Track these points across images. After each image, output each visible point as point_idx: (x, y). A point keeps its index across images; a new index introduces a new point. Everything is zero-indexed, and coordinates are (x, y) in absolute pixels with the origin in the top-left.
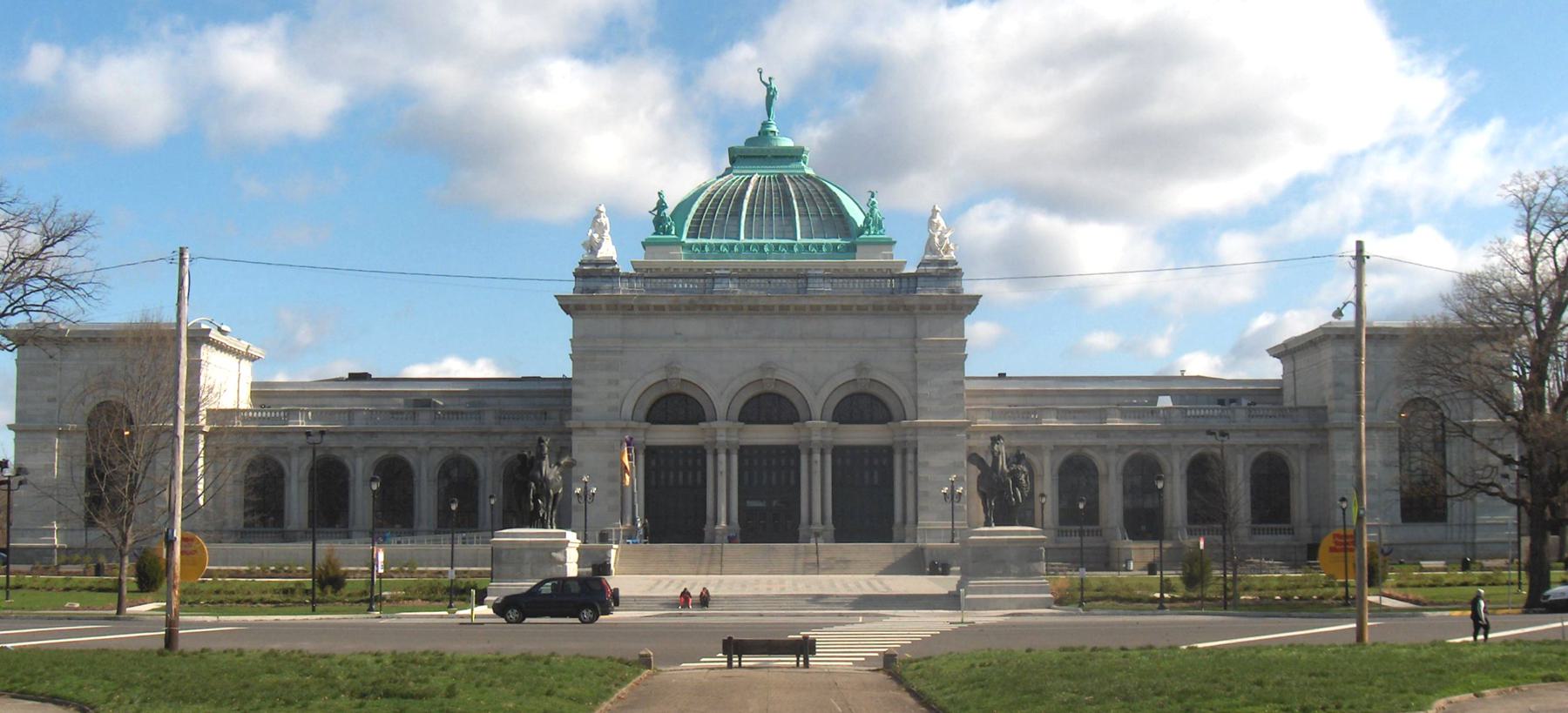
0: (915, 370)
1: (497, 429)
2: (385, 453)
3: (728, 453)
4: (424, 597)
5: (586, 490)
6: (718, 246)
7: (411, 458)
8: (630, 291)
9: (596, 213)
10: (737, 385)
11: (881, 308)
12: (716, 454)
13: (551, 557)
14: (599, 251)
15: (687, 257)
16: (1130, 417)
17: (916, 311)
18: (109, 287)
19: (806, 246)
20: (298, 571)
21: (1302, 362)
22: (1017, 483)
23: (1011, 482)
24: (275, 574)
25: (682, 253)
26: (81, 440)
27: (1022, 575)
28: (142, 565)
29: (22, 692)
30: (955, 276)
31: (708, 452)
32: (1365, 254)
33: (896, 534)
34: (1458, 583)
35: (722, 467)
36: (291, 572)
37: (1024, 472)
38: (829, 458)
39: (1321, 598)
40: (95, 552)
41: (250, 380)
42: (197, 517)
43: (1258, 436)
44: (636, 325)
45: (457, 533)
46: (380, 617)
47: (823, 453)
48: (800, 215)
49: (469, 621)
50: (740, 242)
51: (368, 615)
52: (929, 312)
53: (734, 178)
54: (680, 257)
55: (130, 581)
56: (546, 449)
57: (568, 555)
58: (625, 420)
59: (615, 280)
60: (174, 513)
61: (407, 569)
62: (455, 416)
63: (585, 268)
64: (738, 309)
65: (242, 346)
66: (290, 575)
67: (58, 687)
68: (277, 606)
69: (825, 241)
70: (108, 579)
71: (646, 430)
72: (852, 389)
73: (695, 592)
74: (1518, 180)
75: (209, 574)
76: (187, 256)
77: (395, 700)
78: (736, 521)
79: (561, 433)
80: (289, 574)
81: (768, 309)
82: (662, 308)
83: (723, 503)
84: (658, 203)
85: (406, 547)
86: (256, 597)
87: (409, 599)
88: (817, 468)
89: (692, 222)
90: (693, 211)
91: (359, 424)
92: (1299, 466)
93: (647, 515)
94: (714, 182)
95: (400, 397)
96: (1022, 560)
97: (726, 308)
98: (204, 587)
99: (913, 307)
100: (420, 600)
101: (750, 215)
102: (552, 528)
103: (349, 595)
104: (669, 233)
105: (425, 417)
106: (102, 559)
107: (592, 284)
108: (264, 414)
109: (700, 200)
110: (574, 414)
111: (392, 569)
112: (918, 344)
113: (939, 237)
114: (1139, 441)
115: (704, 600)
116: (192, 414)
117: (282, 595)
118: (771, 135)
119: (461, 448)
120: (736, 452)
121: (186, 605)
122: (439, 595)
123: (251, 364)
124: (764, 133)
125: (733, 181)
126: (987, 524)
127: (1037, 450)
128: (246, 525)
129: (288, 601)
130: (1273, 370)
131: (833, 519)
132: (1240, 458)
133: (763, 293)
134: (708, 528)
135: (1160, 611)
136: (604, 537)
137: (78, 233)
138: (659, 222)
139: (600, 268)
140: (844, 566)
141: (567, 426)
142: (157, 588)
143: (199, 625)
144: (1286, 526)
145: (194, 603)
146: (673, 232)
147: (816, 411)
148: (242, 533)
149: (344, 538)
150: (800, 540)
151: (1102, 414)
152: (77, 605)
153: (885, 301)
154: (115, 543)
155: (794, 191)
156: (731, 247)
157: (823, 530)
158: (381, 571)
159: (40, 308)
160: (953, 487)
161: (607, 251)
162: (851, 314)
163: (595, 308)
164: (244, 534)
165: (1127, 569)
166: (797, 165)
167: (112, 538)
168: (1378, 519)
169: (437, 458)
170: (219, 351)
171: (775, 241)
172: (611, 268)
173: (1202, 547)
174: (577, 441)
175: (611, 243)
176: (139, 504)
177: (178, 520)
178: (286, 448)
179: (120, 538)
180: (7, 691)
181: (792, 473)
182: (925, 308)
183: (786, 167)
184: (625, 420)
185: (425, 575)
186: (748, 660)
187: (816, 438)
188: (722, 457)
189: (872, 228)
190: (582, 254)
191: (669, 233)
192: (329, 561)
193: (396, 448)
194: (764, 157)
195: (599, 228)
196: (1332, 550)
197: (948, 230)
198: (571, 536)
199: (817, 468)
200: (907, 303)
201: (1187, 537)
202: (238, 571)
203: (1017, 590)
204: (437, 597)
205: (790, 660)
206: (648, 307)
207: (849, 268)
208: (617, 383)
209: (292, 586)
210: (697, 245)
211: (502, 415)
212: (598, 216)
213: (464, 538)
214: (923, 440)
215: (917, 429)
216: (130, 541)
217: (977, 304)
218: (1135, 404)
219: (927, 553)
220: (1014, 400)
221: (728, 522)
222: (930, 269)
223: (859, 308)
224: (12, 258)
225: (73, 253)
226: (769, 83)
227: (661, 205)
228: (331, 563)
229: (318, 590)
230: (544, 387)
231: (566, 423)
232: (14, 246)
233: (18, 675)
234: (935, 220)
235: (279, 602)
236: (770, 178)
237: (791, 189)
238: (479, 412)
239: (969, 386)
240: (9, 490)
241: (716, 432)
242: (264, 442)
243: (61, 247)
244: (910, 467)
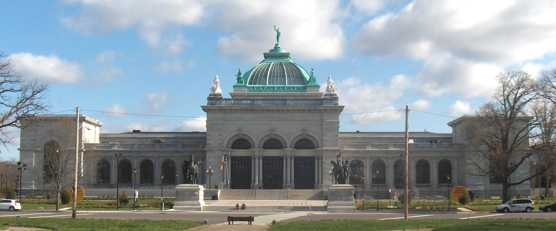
1: (182, 150)
2: (143, 158)
3: (259, 159)
4: (153, 206)
5: (210, 172)
6: (259, 87)
7: (153, 160)
8: (226, 104)
9: (215, 78)
10: (262, 136)
11: (311, 110)
12: (255, 159)
13: (194, 193)
14: (216, 91)
15: (248, 91)
16: (396, 147)
17: (323, 111)
18: (53, 107)
19: (289, 87)
20: (115, 198)
21: (458, 128)
22: (345, 170)
23: (343, 170)
24: (107, 199)
25: (246, 89)
26: (42, 154)
27: (346, 200)
28: (63, 196)
29: (38, 226)
30: (336, 100)
32: (408, 109)
34: (493, 204)
35: (257, 164)
36: (112, 198)
37: (348, 167)
38: (293, 161)
39: (442, 208)
40: (47, 191)
41: (99, 133)
42: (81, 180)
43: (440, 154)
44: (228, 116)
45: (164, 185)
46: (136, 212)
47: (291, 159)
49: (162, 212)
51: (133, 211)
52: (327, 111)
53: (266, 63)
54: (246, 91)
55: (60, 201)
56: (193, 159)
57: (200, 193)
58: (224, 148)
59: (221, 101)
60: (75, 181)
61: (150, 197)
62: (168, 146)
63: (211, 97)
64: (262, 111)
65: (96, 122)
66: (111, 199)
67: (47, 225)
68: (106, 208)
69: (295, 86)
70: (52, 200)
71: (231, 151)
72: (301, 138)
73: (240, 205)
74: (501, 74)
75: (85, 199)
76: (79, 109)
77: (129, 227)
78: (262, 182)
79: (203, 152)
80: (111, 199)
81: (273, 111)
82: (237, 110)
83: (257, 176)
85: (148, 190)
86: (100, 206)
87: (149, 207)
88: (289, 164)
90: (251, 75)
91: (135, 148)
92: (455, 164)
93: (232, 180)
94: (258, 65)
95: (150, 139)
96: (346, 195)
97: (258, 110)
98: (83, 203)
99: (321, 110)
100: (152, 207)
101: (270, 77)
102: (195, 184)
103: (129, 205)
104: (242, 83)
105: (157, 146)
106: (49, 194)
107: (213, 102)
108: (105, 145)
109: (253, 71)
110: (207, 146)
111: (146, 197)
112: (323, 122)
113: (331, 86)
115: (244, 207)
116: (80, 145)
117: (108, 206)
118: (278, 48)
119: (169, 157)
121: (77, 208)
122: (158, 206)
123: (99, 127)
124: (276, 48)
125: (265, 65)
126: (336, 184)
127: (364, 158)
128: (97, 183)
129: (110, 207)
130: (449, 130)
131: (294, 181)
132: (434, 161)
133: (271, 105)
135: (378, 211)
136: (216, 187)
137: (44, 90)
138: (239, 79)
139: (216, 96)
140: (296, 197)
141: (205, 150)
142: (68, 203)
143: (81, 213)
144: (428, 184)
145: (80, 208)
146: (244, 83)
147: (289, 145)
148: (96, 185)
149: (130, 187)
150: (315, 188)
151: (387, 146)
152: (43, 208)
153: (312, 108)
154: (56, 189)
155: (286, 68)
156: (263, 88)
157: (291, 185)
158: (137, 197)
159: (32, 116)
161: (219, 91)
162: (301, 112)
163: (214, 110)
164: (96, 186)
165: (393, 199)
167: (55, 187)
168: (481, 182)
169: (161, 160)
170: (88, 124)
171: (279, 86)
172: (220, 96)
173: (390, 192)
174: (208, 155)
175: (220, 88)
176: (63, 176)
177: (76, 183)
178: (111, 157)
179: (57, 187)
180: (33, 226)
182: (325, 110)
183: (283, 60)
184: (224, 148)
185: (157, 199)
186: (235, 223)
187: (289, 154)
188: (257, 160)
189: (312, 81)
190: (210, 92)
191: (242, 83)
192: (123, 195)
193: (148, 157)
195: (216, 83)
196: (455, 193)
197: (334, 84)
198: (201, 187)
199: (289, 164)
200: (319, 109)
201: (415, 188)
202: (94, 198)
203: (344, 205)
204: (158, 206)
205: (247, 223)
206: (232, 110)
207: (304, 95)
208: (221, 135)
209: (112, 203)
210: (252, 87)
211: (183, 146)
212: (216, 79)
213: (170, 187)
214: (324, 155)
215: (322, 151)
216: (60, 188)
217: (343, 109)
218: (401, 142)
220: (360, 141)
221: (259, 182)
222: (328, 97)
223: (303, 110)
224: (23, 99)
225: (42, 97)
227: (239, 74)
228: (124, 195)
229: (119, 204)
230: (199, 136)
231: (204, 148)
232: (23, 95)
233: (36, 223)
234: (329, 80)
235: (107, 208)
236: (277, 64)
237: (284, 67)
238: (176, 145)
239: (340, 135)
240: (21, 171)
241: (255, 152)
242: (104, 155)
243: (38, 95)
244: (320, 164)
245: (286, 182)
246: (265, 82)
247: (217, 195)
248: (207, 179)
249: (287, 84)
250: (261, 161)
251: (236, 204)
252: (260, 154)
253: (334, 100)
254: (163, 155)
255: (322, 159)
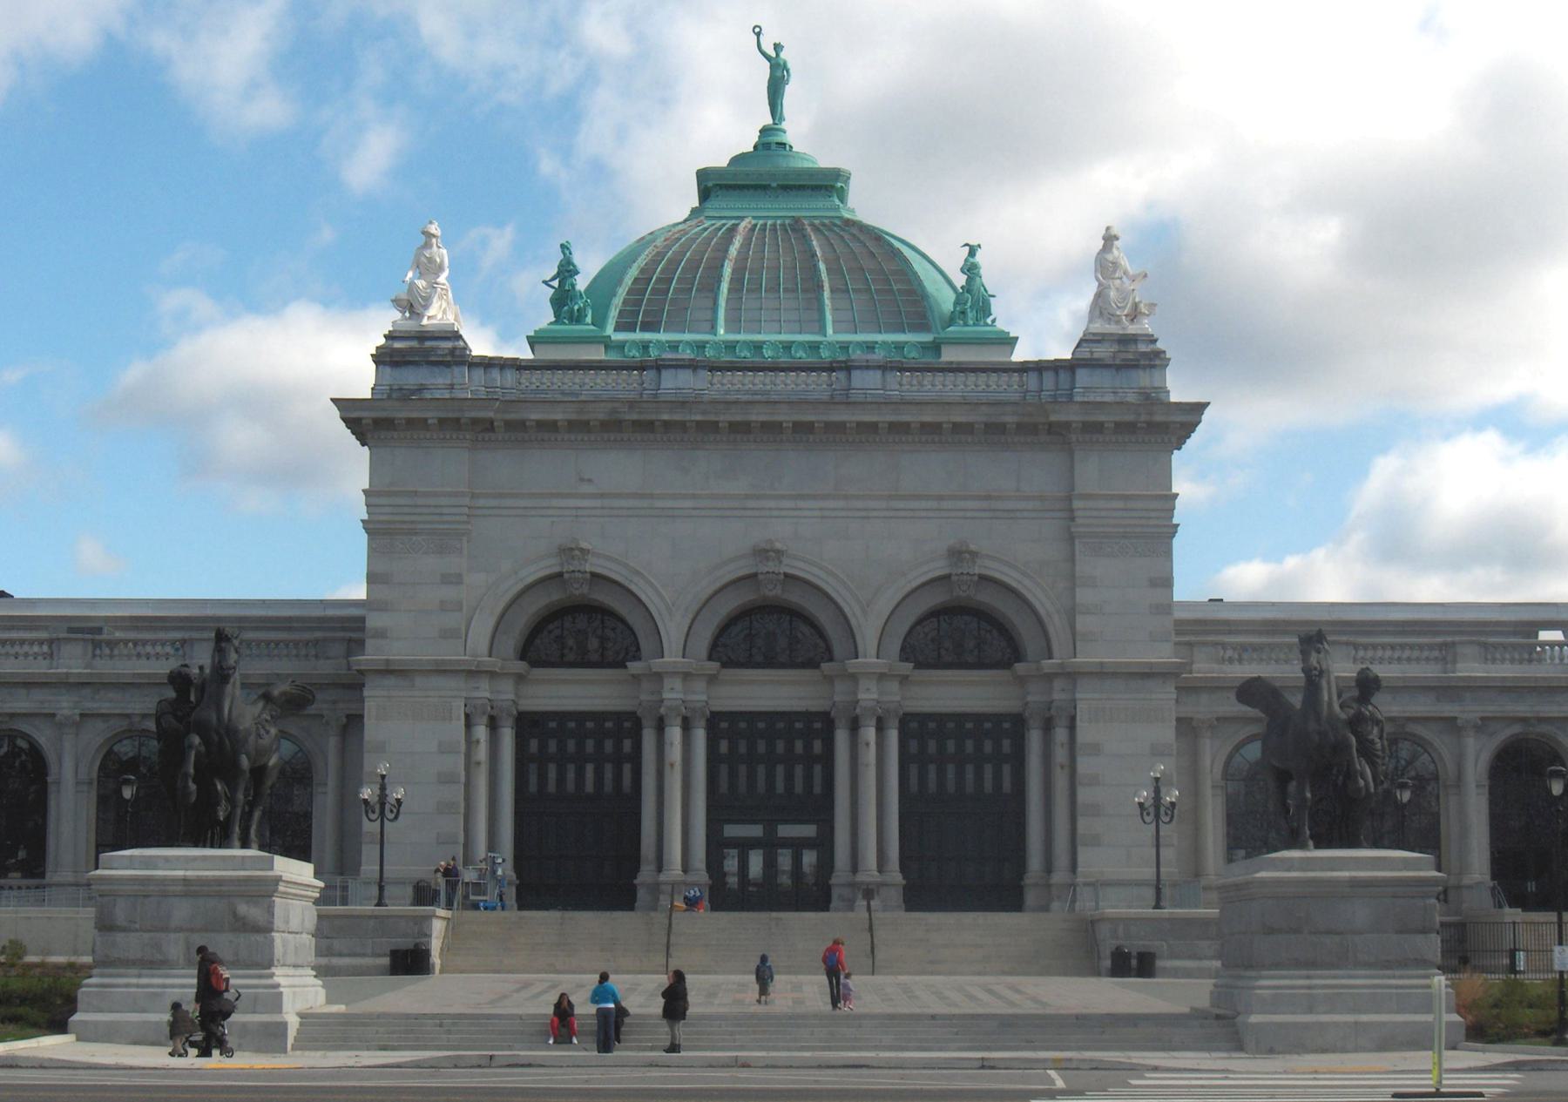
0: (1072, 559)
3: (687, 726)
10: (707, 587)
30: (1153, 366)
31: (644, 722)
33: (1030, 897)
35: (675, 753)
38: (893, 736)
48: (832, 291)
50: (716, 339)
69: (879, 338)
84: (561, 266)
88: (870, 756)
89: (625, 302)
99: (1067, 425)
101: (737, 280)
107: (410, 377)
110: (370, 644)
114: (1523, 708)
120: (703, 723)
124: (770, 142)
125: (706, 229)
134: (645, 874)
138: (563, 299)
139: (428, 344)
146: (589, 319)
160: (1157, 791)
166: (828, 204)
172: (449, 345)
181: (818, 769)
188: (675, 734)
193: (12, 716)
194: (765, 188)
198: (296, 872)
199: (870, 756)
200: (1053, 418)
212: (428, 245)
219: (1104, 931)
226: (774, 55)
227: (567, 270)
244: (1060, 755)
245: (855, 868)
246: (708, 315)
247: (429, 943)
248: (365, 848)
249: (830, 331)
250: (700, 736)
251: (554, 998)
252: (690, 697)
253: (1145, 367)
254: (105, 707)
255: (1072, 727)
